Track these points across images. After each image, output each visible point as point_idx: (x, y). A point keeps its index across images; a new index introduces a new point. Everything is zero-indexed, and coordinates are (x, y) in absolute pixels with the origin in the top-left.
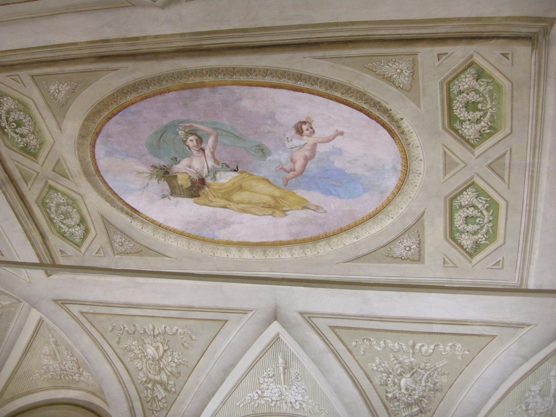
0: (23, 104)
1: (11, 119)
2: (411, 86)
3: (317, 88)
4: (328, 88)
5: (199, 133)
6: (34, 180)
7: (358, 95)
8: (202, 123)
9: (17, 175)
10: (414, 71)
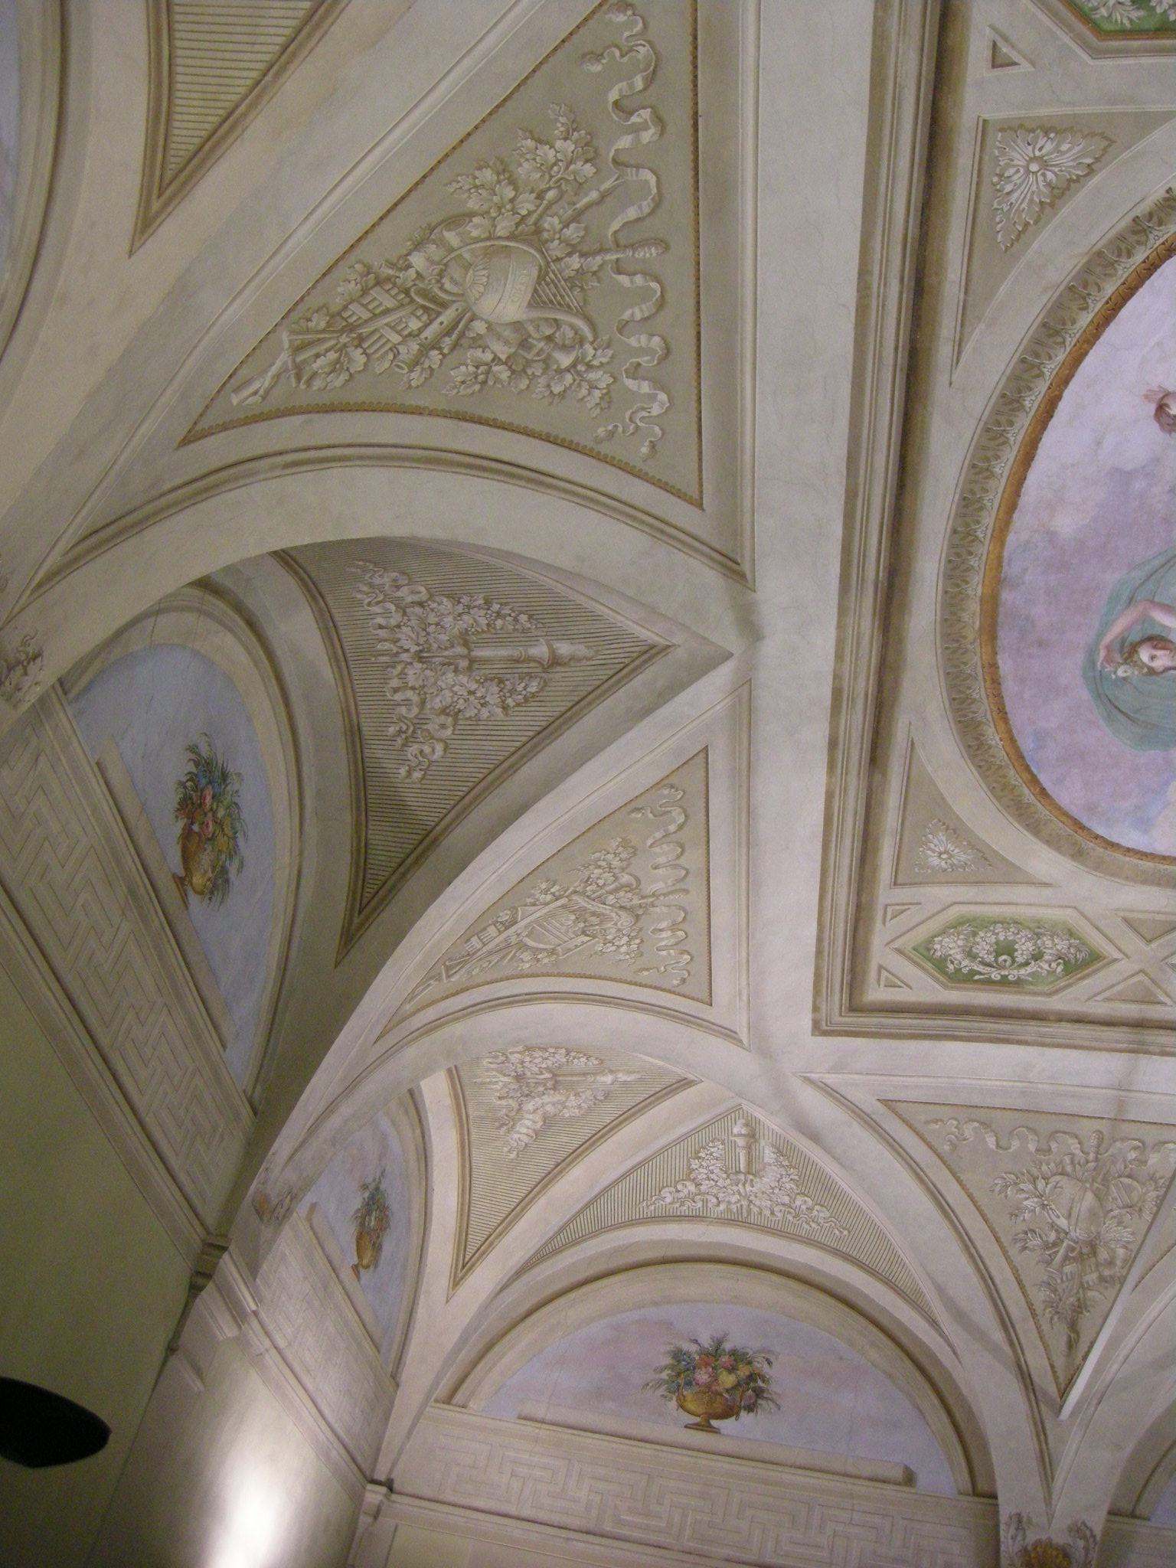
0: (962, 924)
1: (991, 958)
2: (1093, 135)
3: (1051, 368)
4: (1060, 340)
5: (1135, 637)
6: (1159, 987)
7: (1098, 270)
8: (1106, 625)
9: (1131, 1011)
10: (1041, 127)
